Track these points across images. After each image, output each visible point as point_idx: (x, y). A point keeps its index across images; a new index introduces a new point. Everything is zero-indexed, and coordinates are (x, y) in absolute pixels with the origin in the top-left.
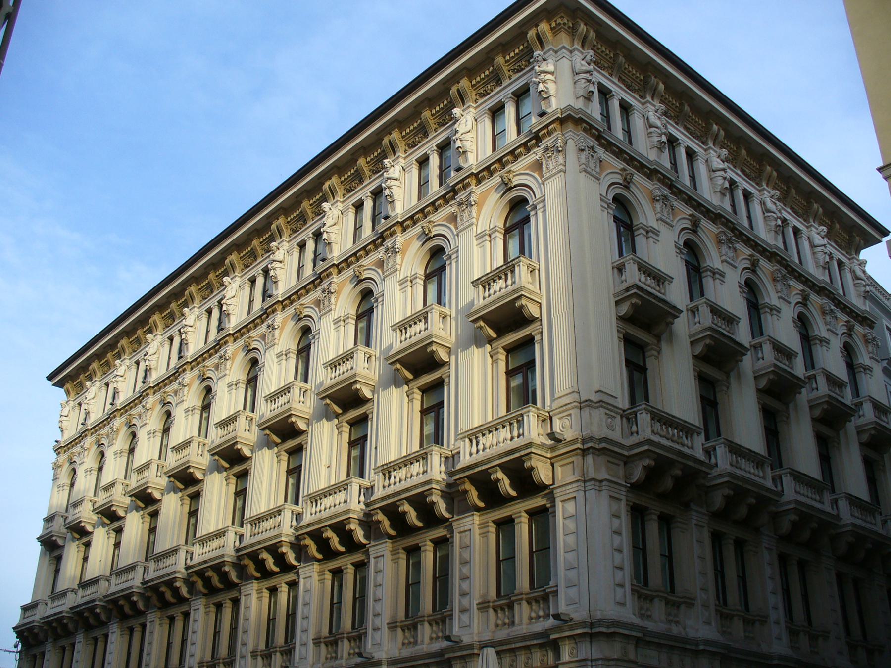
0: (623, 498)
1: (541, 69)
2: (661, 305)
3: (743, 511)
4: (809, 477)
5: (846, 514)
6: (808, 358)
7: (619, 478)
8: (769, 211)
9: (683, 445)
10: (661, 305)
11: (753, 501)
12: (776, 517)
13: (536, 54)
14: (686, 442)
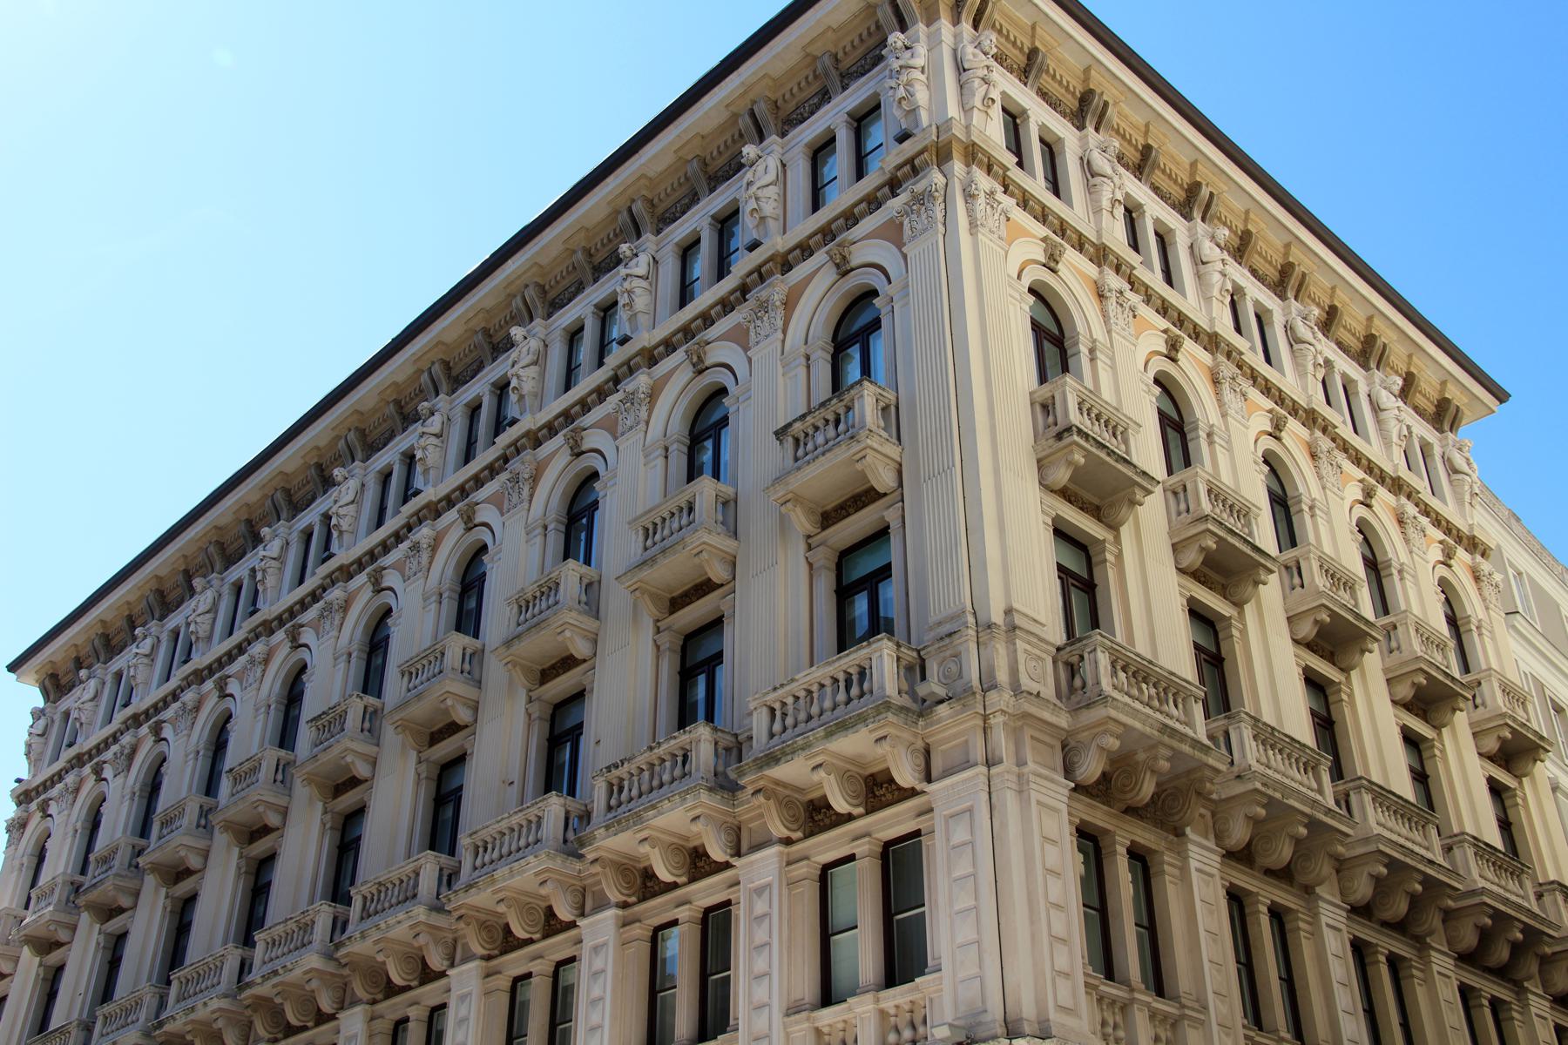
0: (1064, 808)
1: (901, 62)
2: (1119, 466)
3: (1401, 907)
4: (1400, 797)
5: (1478, 876)
6: (1283, 527)
7: (1054, 770)
8: (1456, 471)
9: (1172, 718)
10: (1119, 466)
11: (1303, 831)
12: (1218, 813)
13: (891, 39)
14: (1175, 712)
